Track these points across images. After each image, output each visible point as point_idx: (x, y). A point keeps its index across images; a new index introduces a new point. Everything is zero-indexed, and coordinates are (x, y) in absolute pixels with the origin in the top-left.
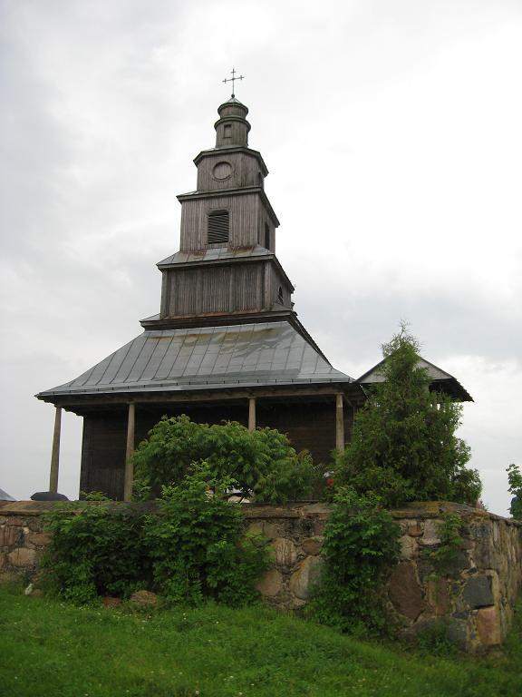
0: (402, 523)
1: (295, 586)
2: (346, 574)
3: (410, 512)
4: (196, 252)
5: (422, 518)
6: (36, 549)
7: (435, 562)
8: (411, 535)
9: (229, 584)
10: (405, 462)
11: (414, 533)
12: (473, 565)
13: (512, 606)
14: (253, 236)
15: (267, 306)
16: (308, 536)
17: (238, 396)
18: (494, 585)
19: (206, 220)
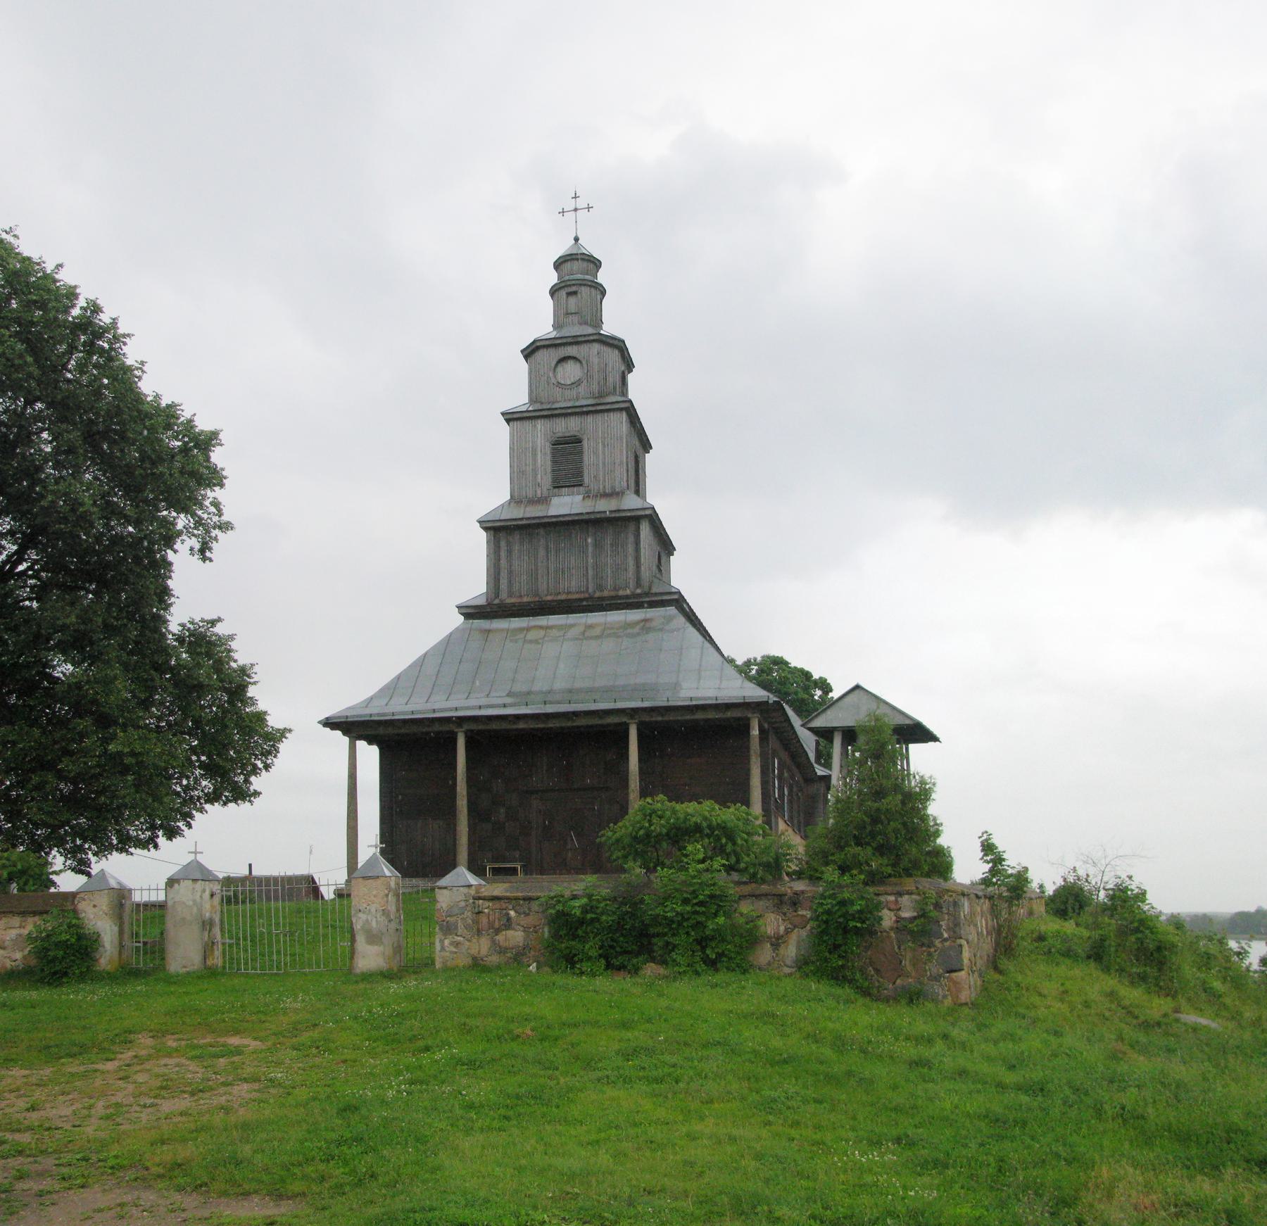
0: (882, 899)
1: (784, 956)
2: (834, 944)
3: (889, 889)
4: (533, 501)
5: (900, 894)
6: (524, 931)
7: (911, 932)
8: (890, 910)
9: (726, 956)
10: (881, 841)
11: (893, 907)
12: (946, 935)
13: (980, 976)
14: (621, 478)
15: (646, 584)
16: (796, 912)
17: (445, 728)
18: (964, 952)
19: (548, 451)
